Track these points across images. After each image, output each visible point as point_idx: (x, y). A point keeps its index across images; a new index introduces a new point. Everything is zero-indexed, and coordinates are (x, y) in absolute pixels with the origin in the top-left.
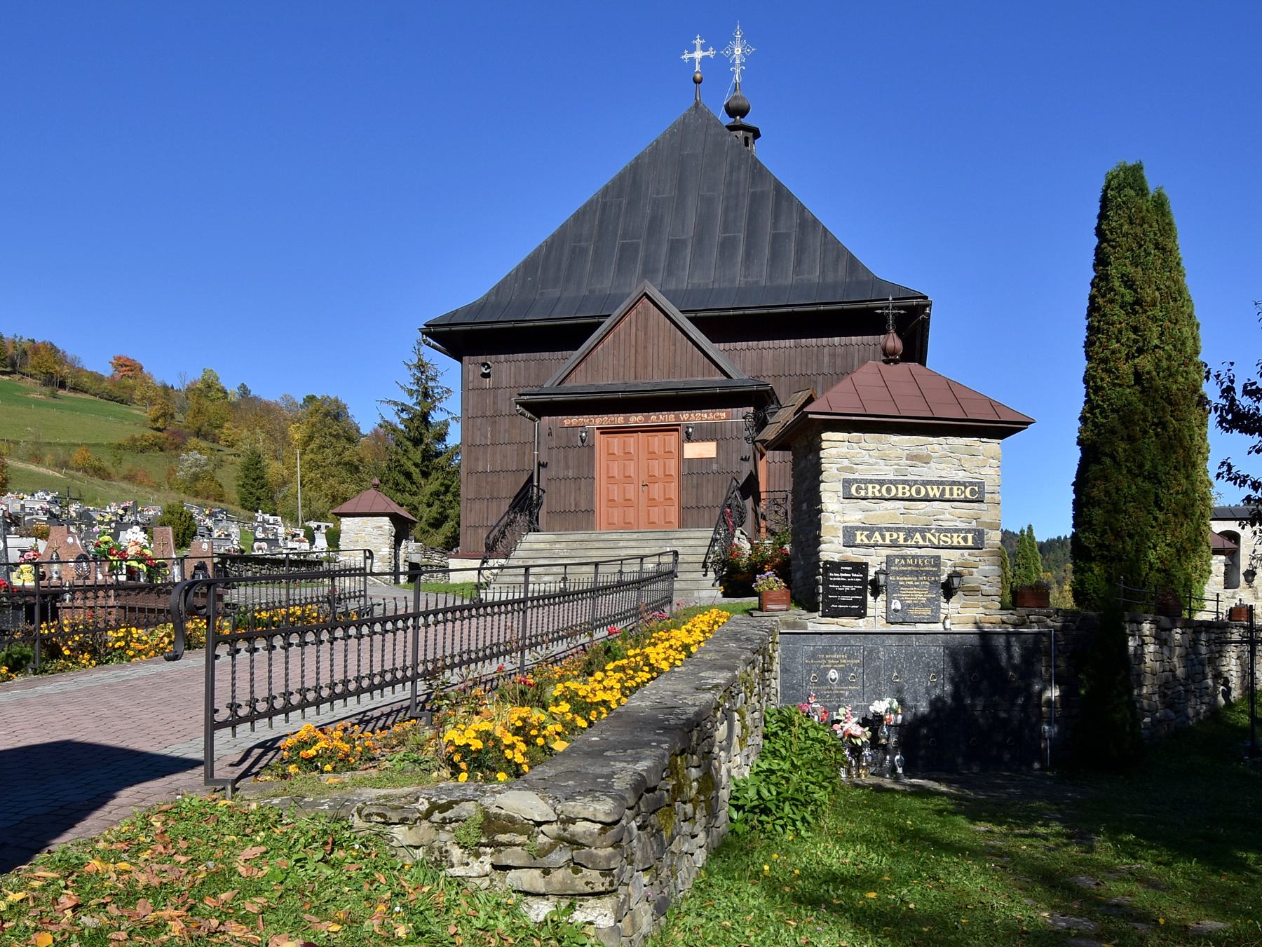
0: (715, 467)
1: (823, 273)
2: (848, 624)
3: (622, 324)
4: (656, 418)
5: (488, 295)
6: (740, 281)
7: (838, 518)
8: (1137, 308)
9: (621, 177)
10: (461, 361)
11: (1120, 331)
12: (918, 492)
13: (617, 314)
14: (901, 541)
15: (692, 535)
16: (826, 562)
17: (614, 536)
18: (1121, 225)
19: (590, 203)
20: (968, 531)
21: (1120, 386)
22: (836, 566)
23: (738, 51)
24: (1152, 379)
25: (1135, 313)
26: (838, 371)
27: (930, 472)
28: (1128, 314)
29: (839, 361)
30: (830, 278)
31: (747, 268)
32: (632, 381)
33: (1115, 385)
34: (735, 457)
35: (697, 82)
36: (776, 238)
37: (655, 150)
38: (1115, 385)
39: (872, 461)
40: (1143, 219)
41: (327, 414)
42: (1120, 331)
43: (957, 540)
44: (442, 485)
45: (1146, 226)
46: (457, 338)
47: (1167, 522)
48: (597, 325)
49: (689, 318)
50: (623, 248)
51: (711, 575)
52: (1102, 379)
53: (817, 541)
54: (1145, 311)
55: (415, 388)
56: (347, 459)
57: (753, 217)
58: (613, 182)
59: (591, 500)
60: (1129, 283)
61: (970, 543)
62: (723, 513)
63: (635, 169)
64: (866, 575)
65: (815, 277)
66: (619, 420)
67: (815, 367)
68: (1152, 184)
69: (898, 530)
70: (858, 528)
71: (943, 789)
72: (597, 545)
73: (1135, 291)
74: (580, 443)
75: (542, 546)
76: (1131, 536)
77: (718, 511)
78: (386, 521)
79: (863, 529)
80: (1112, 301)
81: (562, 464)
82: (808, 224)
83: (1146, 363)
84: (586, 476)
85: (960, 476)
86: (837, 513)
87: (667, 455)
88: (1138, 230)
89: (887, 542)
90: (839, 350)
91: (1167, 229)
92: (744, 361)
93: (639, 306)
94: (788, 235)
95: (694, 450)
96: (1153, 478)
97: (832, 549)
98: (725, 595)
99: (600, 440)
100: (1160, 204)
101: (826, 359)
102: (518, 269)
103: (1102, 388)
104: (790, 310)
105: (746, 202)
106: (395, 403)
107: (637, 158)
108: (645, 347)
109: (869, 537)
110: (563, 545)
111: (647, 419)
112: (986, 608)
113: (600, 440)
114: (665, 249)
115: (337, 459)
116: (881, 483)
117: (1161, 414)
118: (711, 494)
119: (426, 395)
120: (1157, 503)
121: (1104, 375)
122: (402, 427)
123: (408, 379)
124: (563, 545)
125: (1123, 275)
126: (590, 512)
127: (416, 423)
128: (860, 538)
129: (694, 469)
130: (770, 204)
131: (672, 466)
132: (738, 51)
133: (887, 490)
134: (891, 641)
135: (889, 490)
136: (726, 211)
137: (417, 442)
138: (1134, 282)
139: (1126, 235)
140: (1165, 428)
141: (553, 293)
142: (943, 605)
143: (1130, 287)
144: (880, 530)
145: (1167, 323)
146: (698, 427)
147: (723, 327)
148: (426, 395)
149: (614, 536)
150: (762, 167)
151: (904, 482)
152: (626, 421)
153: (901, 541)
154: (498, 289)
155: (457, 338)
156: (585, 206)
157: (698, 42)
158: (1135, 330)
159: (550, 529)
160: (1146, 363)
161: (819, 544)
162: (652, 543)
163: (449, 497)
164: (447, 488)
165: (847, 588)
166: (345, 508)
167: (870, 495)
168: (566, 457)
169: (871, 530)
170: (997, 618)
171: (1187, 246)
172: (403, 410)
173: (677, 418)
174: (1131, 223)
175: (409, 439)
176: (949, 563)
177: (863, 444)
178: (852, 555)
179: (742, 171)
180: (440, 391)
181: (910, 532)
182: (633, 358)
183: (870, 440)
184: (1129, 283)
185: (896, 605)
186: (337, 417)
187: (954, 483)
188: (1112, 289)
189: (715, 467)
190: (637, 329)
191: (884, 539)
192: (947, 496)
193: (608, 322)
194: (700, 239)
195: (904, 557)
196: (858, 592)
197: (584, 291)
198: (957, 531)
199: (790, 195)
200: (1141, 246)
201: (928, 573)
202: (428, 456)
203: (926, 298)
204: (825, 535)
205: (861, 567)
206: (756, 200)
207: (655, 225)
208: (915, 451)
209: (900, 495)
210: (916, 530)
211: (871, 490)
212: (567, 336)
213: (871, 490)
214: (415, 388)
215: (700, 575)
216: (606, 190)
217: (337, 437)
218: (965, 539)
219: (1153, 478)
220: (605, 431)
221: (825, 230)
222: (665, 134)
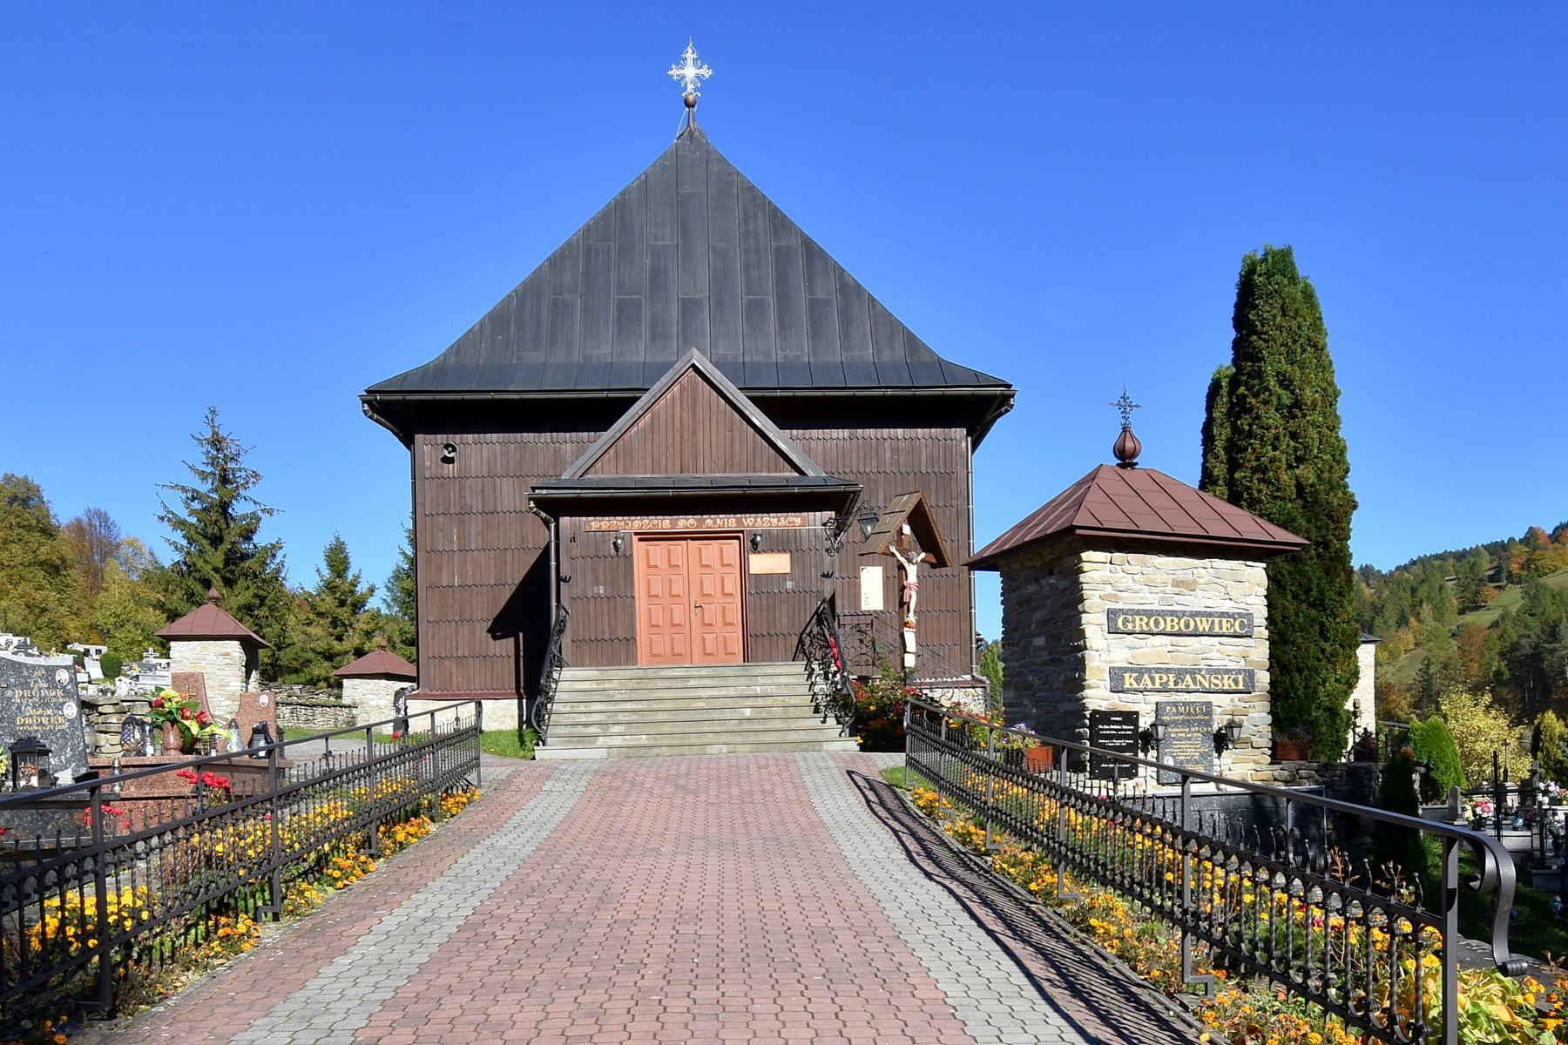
0: (789, 584)
1: (877, 350)
3: (662, 402)
4: (712, 522)
5: (445, 355)
6: (777, 355)
7: (1104, 657)
8: (1297, 411)
9: (604, 216)
10: (408, 441)
11: (1277, 438)
12: (1187, 626)
13: (656, 388)
14: (1172, 685)
15: (777, 670)
16: (1095, 712)
17: (678, 673)
18: (1275, 316)
19: (569, 244)
20: (1239, 672)
21: (1282, 499)
22: (1102, 717)
24: (1317, 492)
25: (1294, 417)
26: (903, 470)
27: (1195, 602)
28: (1284, 417)
29: (903, 457)
30: (887, 356)
31: (784, 339)
32: (678, 475)
33: (1275, 498)
34: (814, 573)
35: (688, 105)
36: (814, 305)
37: (645, 185)
38: (1275, 498)
39: (1137, 587)
40: (1297, 311)
41: (15, 498)
42: (1277, 438)
43: (1227, 683)
44: (256, 596)
45: (1300, 319)
46: (407, 412)
47: (1334, 655)
48: (634, 400)
49: (750, 398)
50: (621, 306)
51: (831, 721)
52: (1259, 491)
53: (1080, 685)
54: (1304, 416)
55: (209, 469)
56: (43, 557)
57: (781, 280)
58: (596, 220)
59: (632, 627)
60: (1286, 383)
61: (1241, 687)
62: (801, 641)
63: (620, 206)
64: (1137, 727)
65: (868, 354)
66: (664, 523)
67: (874, 463)
68: (1302, 270)
69: (1168, 671)
70: (1125, 670)
72: (660, 684)
73: (1292, 392)
74: (613, 551)
75: (586, 685)
76: (1300, 670)
77: (795, 640)
78: (234, 647)
79: (1131, 670)
80: (1266, 403)
81: (589, 579)
82: (850, 291)
83: (1307, 473)
84: (622, 595)
85: (1227, 606)
86: (1103, 652)
87: (725, 570)
88: (1294, 324)
89: (1158, 686)
90: (902, 445)
91: (1317, 325)
92: (816, 453)
93: (684, 379)
94: (828, 302)
95: (761, 564)
96: (1319, 604)
97: (1097, 696)
98: (863, 748)
99: (639, 548)
100: (1308, 296)
101: (888, 455)
102: (482, 324)
103: (1260, 501)
104: (850, 393)
105: (770, 259)
106: (184, 489)
107: (623, 193)
108: (694, 433)
109: (1138, 680)
110: (614, 685)
111: (701, 523)
112: (1256, 762)
113: (639, 548)
114: (674, 311)
115: (31, 556)
116: (1149, 614)
117: (1324, 532)
118: (785, 619)
119: (225, 480)
120: (1323, 632)
121: (1263, 486)
122: (193, 520)
123: (199, 456)
124: (614, 685)
125: (1278, 373)
126: (630, 640)
127: (214, 516)
128: (1129, 681)
129: (754, 588)
130: (800, 262)
131: (733, 584)
133: (1157, 622)
135: (1157, 623)
136: (747, 267)
137: (216, 541)
138: (1291, 382)
139: (1280, 328)
140: (1327, 548)
141: (535, 357)
142: (1216, 761)
143: (1286, 388)
144: (1149, 670)
145: (1324, 430)
146: (767, 534)
147: (792, 411)
148: (225, 480)
149: (678, 673)
150: (784, 217)
151: (1172, 613)
152: (673, 524)
153: (1172, 685)
154: (458, 347)
155: (407, 412)
156: (563, 249)
157: (690, 55)
158: (1294, 436)
159: (579, 663)
160: (1307, 473)
161: (1083, 688)
162: (731, 681)
163: (264, 612)
164: (263, 600)
165: (1117, 743)
166: (178, 627)
167: (1138, 629)
168: (594, 570)
169: (1140, 672)
170: (1267, 774)
171: (1335, 346)
172: (193, 499)
173: (739, 522)
174: (1284, 315)
175: (205, 537)
176: (1219, 710)
177: (1127, 567)
179: (760, 220)
180: (243, 474)
181: (1180, 674)
182: (678, 446)
184: (1286, 383)
186: (25, 502)
187: (1222, 615)
188: (1267, 389)
189: (789, 584)
190: (682, 409)
191: (1153, 683)
192: (1217, 630)
193: (645, 398)
194: (720, 300)
195: (1175, 704)
196: (1130, 748)
197: (577, 358)
198: (1228, 671)
199: (823, 256)
200: (1295, 342)
201: (1200, 722)
202: (234, 558)
203: (1009, 386)
204: (1091, 677)
205: (1131, 717)
206: (782, 257)
207: (657, 279)
208: (1181, 576)
209: (1169, 629)
210: (1186, 671)
212: (596, 412)
214: (209, 469)
215: (817, 722)
216: (587, 231)
217: (29, 528)
218: (1236, 682)
219: (1319, 604)
220: (645, 537)
221: (872, 300)
222: (654, 165)
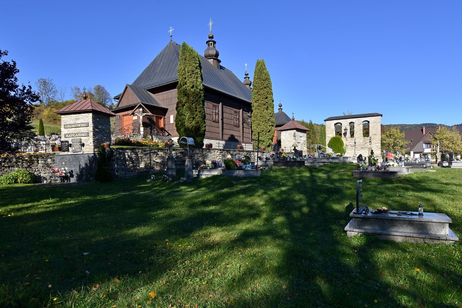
2: (66, 153)
23: (211, 24)
71: (164, 188)
128: (67, 136)
132: (211, 24)
134: (73, 156)
157: (171, 28)
169: (69, 134)
178: (66, 139)
181: (75, 134)
183: (69, 116)
185: (73, 149)
205: (67, 142)
211: (68, 126)
213: (68, 126)
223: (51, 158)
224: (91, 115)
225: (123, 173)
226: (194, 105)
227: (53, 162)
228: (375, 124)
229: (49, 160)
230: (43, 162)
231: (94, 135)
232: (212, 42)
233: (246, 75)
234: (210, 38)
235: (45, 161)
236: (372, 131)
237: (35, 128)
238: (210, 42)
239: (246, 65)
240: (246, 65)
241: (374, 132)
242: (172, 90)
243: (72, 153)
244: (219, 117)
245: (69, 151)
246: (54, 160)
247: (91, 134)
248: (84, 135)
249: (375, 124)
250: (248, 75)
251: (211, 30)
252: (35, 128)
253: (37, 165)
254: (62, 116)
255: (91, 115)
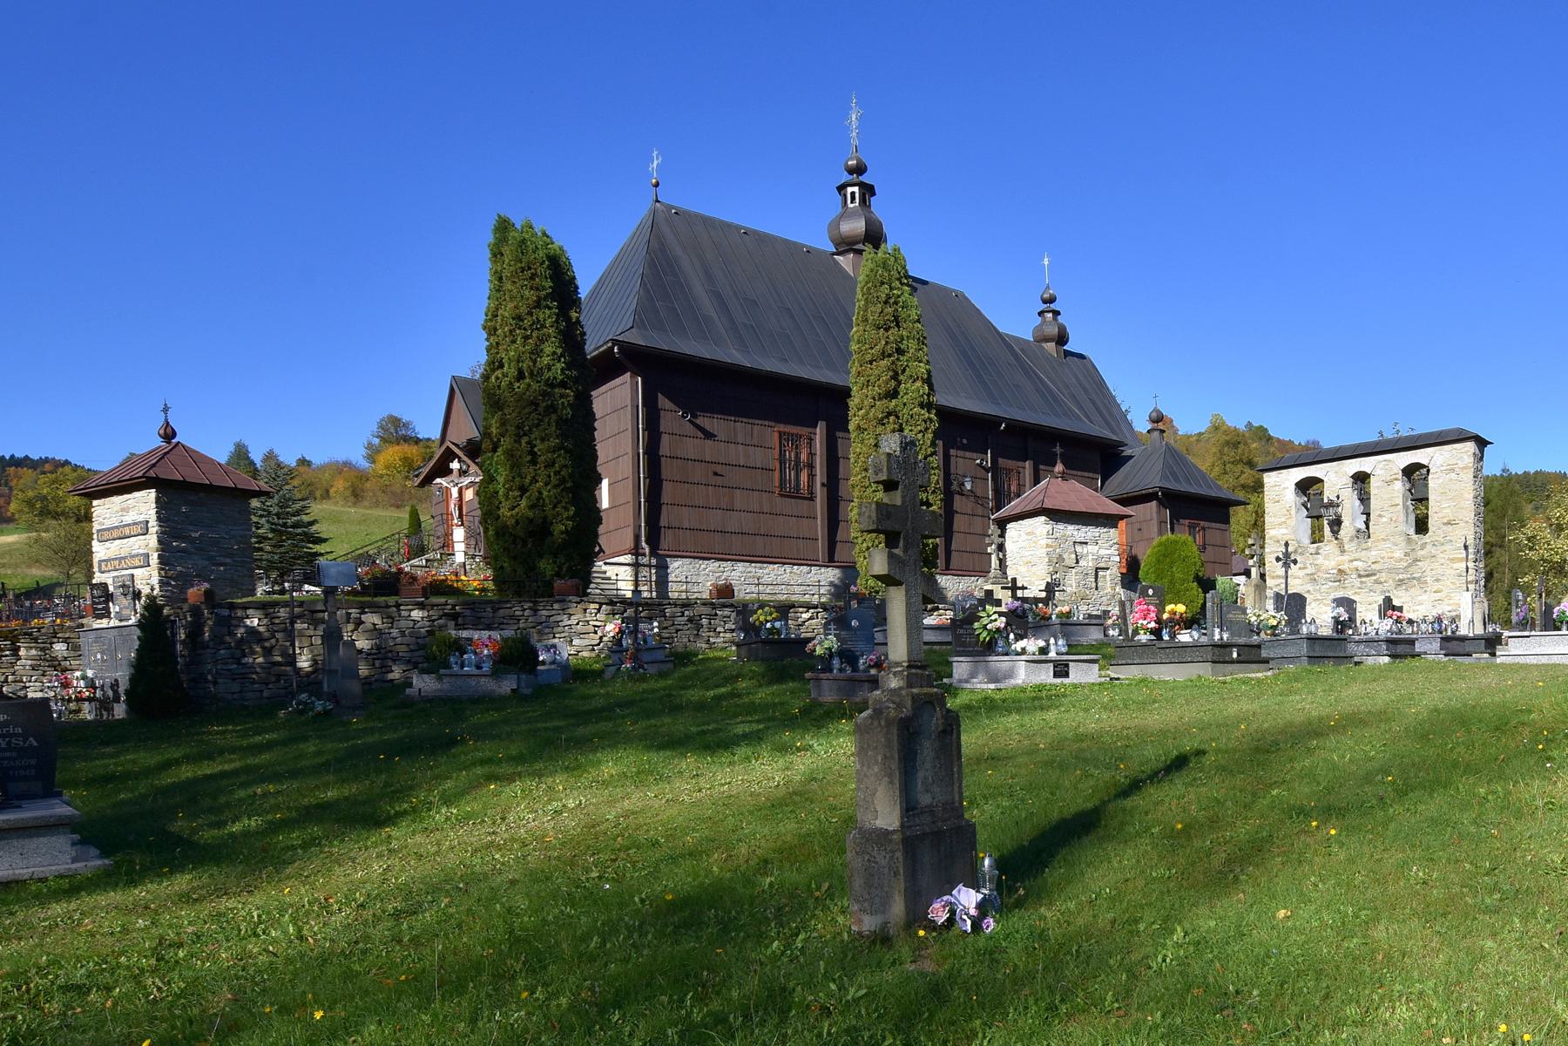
2: (104, 623)
223: (65, 640)
224: (151, 494)
225: (236, 687)
226: (524, 440)
227: (72, 654)
228: (1452, 472)
229: (59, 648)
230: (34, 652)
231: (163, 560)
232: (856, 189)
233: (1045, 302)
234: (851, 171)
235: (43, 649)
236: (1437, 510)
237: (325, 540)
238: (850, 190)
239: (1046, 262)
240: (1046, 262)
241: (1448, 513)
242: (604, 388)
243: (117, 623)
244: (812, 476)
245: (109, 617)
246: (76, 648)
247: (154, 559)
248: (137, 563)
249: (1452, 472)
250: (1052, 300)
251: (855, 142)
252: (325, 540)
253: (13, 665)
254: (95, 503)
255: (151, 494)
